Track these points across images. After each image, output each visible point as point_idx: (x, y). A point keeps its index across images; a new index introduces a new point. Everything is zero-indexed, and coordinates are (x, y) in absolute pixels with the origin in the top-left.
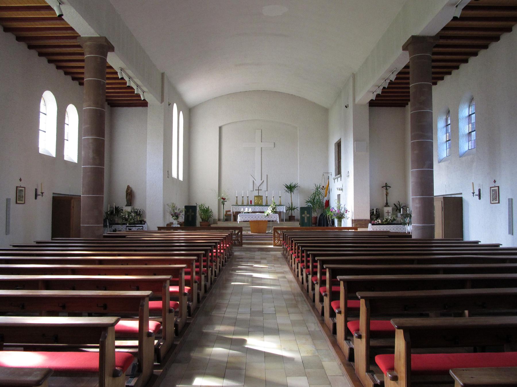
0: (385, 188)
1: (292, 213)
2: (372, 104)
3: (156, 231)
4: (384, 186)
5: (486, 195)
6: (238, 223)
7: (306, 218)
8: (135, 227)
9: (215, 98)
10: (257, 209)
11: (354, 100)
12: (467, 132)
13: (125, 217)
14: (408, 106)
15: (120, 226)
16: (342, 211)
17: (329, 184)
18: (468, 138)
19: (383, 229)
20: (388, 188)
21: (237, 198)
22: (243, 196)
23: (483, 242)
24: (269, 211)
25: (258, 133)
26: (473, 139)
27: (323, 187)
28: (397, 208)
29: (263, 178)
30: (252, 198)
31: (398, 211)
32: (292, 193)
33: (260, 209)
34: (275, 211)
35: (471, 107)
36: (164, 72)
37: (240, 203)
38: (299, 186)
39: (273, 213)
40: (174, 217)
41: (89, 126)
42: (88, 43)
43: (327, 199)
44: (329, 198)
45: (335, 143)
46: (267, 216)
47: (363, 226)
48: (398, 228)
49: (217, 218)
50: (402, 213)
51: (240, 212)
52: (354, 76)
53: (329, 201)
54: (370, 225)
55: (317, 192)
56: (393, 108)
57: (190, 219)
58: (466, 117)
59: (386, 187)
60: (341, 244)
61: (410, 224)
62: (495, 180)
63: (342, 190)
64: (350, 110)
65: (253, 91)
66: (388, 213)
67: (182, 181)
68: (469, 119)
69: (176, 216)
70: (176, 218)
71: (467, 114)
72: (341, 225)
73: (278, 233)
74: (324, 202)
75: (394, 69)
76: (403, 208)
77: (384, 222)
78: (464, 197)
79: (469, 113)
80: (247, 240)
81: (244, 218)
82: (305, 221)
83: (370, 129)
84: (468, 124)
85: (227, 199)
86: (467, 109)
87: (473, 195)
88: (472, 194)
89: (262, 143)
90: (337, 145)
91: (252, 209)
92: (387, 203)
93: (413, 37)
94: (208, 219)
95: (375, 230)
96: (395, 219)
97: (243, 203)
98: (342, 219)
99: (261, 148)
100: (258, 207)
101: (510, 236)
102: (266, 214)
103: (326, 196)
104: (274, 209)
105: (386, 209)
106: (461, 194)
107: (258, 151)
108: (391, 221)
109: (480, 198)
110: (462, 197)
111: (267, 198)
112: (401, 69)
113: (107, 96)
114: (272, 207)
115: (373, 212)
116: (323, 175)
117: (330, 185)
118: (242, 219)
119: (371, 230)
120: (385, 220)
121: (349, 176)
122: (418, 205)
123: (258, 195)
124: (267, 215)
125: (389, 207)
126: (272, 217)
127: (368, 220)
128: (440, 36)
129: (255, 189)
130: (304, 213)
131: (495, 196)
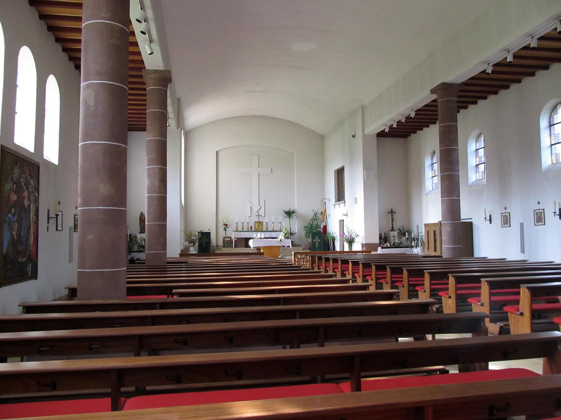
0: (391, 213)
2: (381, 135)
3: (178, 258)
5: (497, 219)
6: (252, 248)
9: (211, 122)
11: (363, 131)
12: (475, 165)
13: (142, 244)
15: (136, 253)
16: (353, 235)
17: (326, 210)
18: (475, 170)
19: (398, 252)
20: (393, 213)
21: (237, 224)
22: (237, 222)
23: (509, 259)
24: (281, 236)
25: (256, 158)
26: (480, 171)
27: (322, 212)
28: (402, 233)
29: (260, 204)
31: (403, 235)
32: (291, 218)
34: (287, 237)
35: (477, 143)
36: (180, 98)
39: (285, 238)
42: (153, 76)
43: (324, 224)
44: (326, 222)
45: (335, 170)
47: (373, 249)
48: (405, 251)
50: (407, 237)
51: (253, 238)
52: (363, 108)
54: (379, 248)
55: (315, 218)
57: (204, 245)
58: (474, 151)
59: (392, 212)
60: (257, 271)
61: (418, 247)
62: (505, 207)
63: (347, 215)
64: (359, 140)
66: (394, 237)
68: (476, 153)
69: (192, 242)
70: (193, 245)
71: (475, 149)
72: (352, 250)
73: (298, 258)
74: (322, 227)
75: (415, 107)
76: (408, 233)
77: (392, 246)
78: (473, 222)
79: (476, 148)
81: (258, 243)
82: (316, 245)
83: (378, 159)
84: (475, 157)
85: (229, 225)
86: (475, 144)
87: (486, 220)
88: (485, 219)
90: (337, 172)
91: (264, 235)
92: (392, 228)
93: (443, 84)
96: (402, 242)
97: (243, 229)
98: (352, 243)
99: (259, 173)
101: (522, 254)
102: (279, 240)
103: (323, 221)
105: (392, 233)
106: (471, 219)
108: (398, 244)
109: (491, 222)
110: (472, 222)
111: (244, 223)
112: (420, 107)
113: (129, 124)
114: (284, 232)
115: (382, 236)
116: (322, 201)
118: (269, 244)
119: (381, 253)
121: (356, 202)
122: (449, 229)
124: (280, 240)
126: (284, 243)
127: (378, 244)
128: (465, 84)
131: (506, 221)
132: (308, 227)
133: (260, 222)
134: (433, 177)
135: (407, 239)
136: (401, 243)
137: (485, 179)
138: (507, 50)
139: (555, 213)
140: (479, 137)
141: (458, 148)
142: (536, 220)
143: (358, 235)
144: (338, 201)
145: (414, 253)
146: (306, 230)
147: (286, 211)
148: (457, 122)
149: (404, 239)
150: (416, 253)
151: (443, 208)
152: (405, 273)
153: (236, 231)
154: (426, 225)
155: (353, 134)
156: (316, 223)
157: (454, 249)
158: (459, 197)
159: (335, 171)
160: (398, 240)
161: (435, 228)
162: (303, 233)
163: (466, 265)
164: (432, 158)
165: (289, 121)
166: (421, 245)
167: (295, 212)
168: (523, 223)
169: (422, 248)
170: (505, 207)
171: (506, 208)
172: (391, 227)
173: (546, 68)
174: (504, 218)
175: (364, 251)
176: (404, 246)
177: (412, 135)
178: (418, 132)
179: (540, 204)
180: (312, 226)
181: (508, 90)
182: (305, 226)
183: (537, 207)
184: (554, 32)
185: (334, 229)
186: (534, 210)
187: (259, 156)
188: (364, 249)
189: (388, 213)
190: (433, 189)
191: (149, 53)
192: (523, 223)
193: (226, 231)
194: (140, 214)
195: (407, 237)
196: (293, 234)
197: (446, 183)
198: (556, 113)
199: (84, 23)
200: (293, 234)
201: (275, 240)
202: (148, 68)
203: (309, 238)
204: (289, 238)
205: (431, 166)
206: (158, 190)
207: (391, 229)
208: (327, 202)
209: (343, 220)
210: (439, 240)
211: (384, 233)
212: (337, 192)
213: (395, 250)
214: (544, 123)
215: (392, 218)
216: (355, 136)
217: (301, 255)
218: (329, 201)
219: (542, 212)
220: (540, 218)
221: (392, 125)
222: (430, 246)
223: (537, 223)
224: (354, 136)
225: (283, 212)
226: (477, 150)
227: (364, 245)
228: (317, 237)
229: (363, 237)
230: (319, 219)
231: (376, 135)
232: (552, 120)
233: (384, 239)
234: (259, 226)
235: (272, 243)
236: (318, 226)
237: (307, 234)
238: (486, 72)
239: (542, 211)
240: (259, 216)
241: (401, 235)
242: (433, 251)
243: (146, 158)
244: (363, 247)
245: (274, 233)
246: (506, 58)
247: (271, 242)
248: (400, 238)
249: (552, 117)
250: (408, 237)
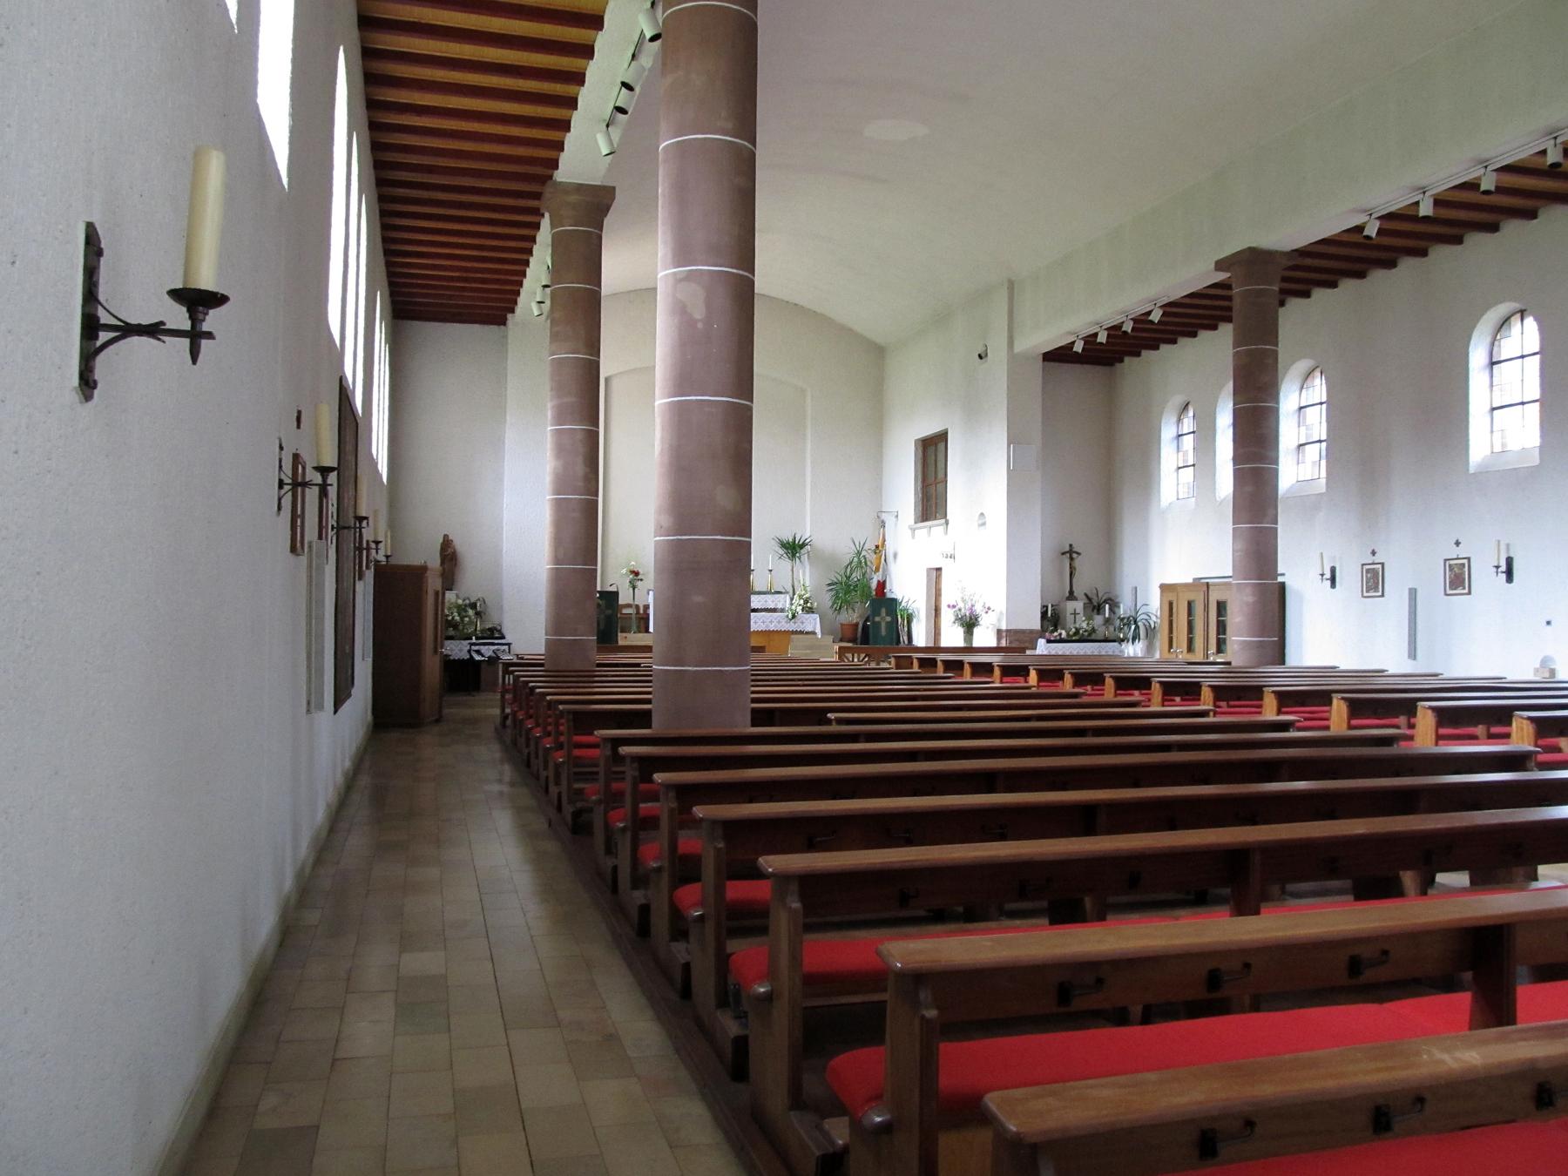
0: (1068, 555)
2: (1059, 356)
4: (1067, 552)
5: (1351, 578)
7: (883, 625)
8: (487, 647)
14: (1122, 364)
16: (978, 609)
17: (884, 541)
18: (1296, 457)
20: (1075, 555)
28: (1094, 607)
34: (810, 608)
35: (1304, 391)
41: (574, 399)
42: (573, 198)
43: (880, 578)
50: (1107, 615)
53: (884, 582)
54: (1041, 642)
55: (859, 562)
56: (1087, 367)
59: (1071, 553)
62: (1373, 550)
64: (998, 368)
72: (972, 644)
74: (874, 585)
86: (1297, 393)
92: (1071, 592)
93: (1252, 250)
95: (1053, 653)
101: (1411, 662)
103: (877, 569)
110: (1284, 583)
120: (1074, 630)
121: (984, 524)
122: (1250, 599)
125: (1077, 600)
126: (803, 623)
127: (1037, 631)
128: (1302, 253)
130: (879, 615)
131: (1374, 581)
134: (1180, 468)
135: (1107, 621)
136: (1094, 630)
137: (1323, 481)
138: (1419, 189)
139: (1497, 567)
140: (1308, 375)
141: (1276, 406)
142: (1450, 582)
143: (989, 608)
144: (923, 521)
145: (1126, 655)
148: (1277, 345)
149: (1098, 620)
150: (1132, 654)
151: (1239, 547)
152: (1207, 694)
154: (1165, 588)
155: (980, 350)
157: (1261, 645)
158: (1276, 523)
159: (916, 441)
160: (1086, 622)
161: (1191, 596)
163: (1276, 678)
164: (1179, 420)
165: (796, 304)
166: (1145, 634)
168: (1415, 589)
169: (1146, 642)
170: (1373, 550)
171: (1374, 553)
172: (1068, 589)
173: (1493, 228)
174: (1369, 575)
175: (1002, 648)
176: (1099, 638)
177: (1127, 359)
178: (1144, 353)
179: (1460, 546)
181: (1394, 270)
183: (1453, 552)
184: (1540, 160)
185: (907, 588)
186: (1446, 560)
188: (1004, 643)
189: (1063, 554)
190: (1178, 499)
191: (605, 152)
192: (1415, 589)
193: (634, 589)
194: (441, 540)
195: (1107, 615)
197: (1249, 489)
198: (1507, 334)
199: (664, 141)
202: (562, 178)
204: (813, 612)
205: (1176, 442)
206: (580, 484)
207: (1067, 594)
209: (939, 570)
210: (1202, 624)
211: (1052, 606)
213: (1071, 647)
214: (1477, 356)
215: (1070, 568)
216: (986, 355)
217: (856, 655)
218: (894, 519)
219: (1463, 565)
220: (1458, 578)
221: (1096, 335)
222: (1174, 640)
223: (1451, 588)
224: (983, 355)
226: (1303, 410)
227: (1004, 634)
228: (883, 611)
229: (1001, 613)
230: (869, 563)
231: (1041, 357)
232: (1495, 349)
233: (1051, 620)
235: (771, 622)
238: (1365, 233)
239: (1465, 561)
241: (1093, 610)
242: (1185, 651)
243: (549, 405)
244: (999, 639)
245: (769, 596)
246: (1417, 203)
248: (1089, 618)
249: (1496, 343)
250: (1109, 615)
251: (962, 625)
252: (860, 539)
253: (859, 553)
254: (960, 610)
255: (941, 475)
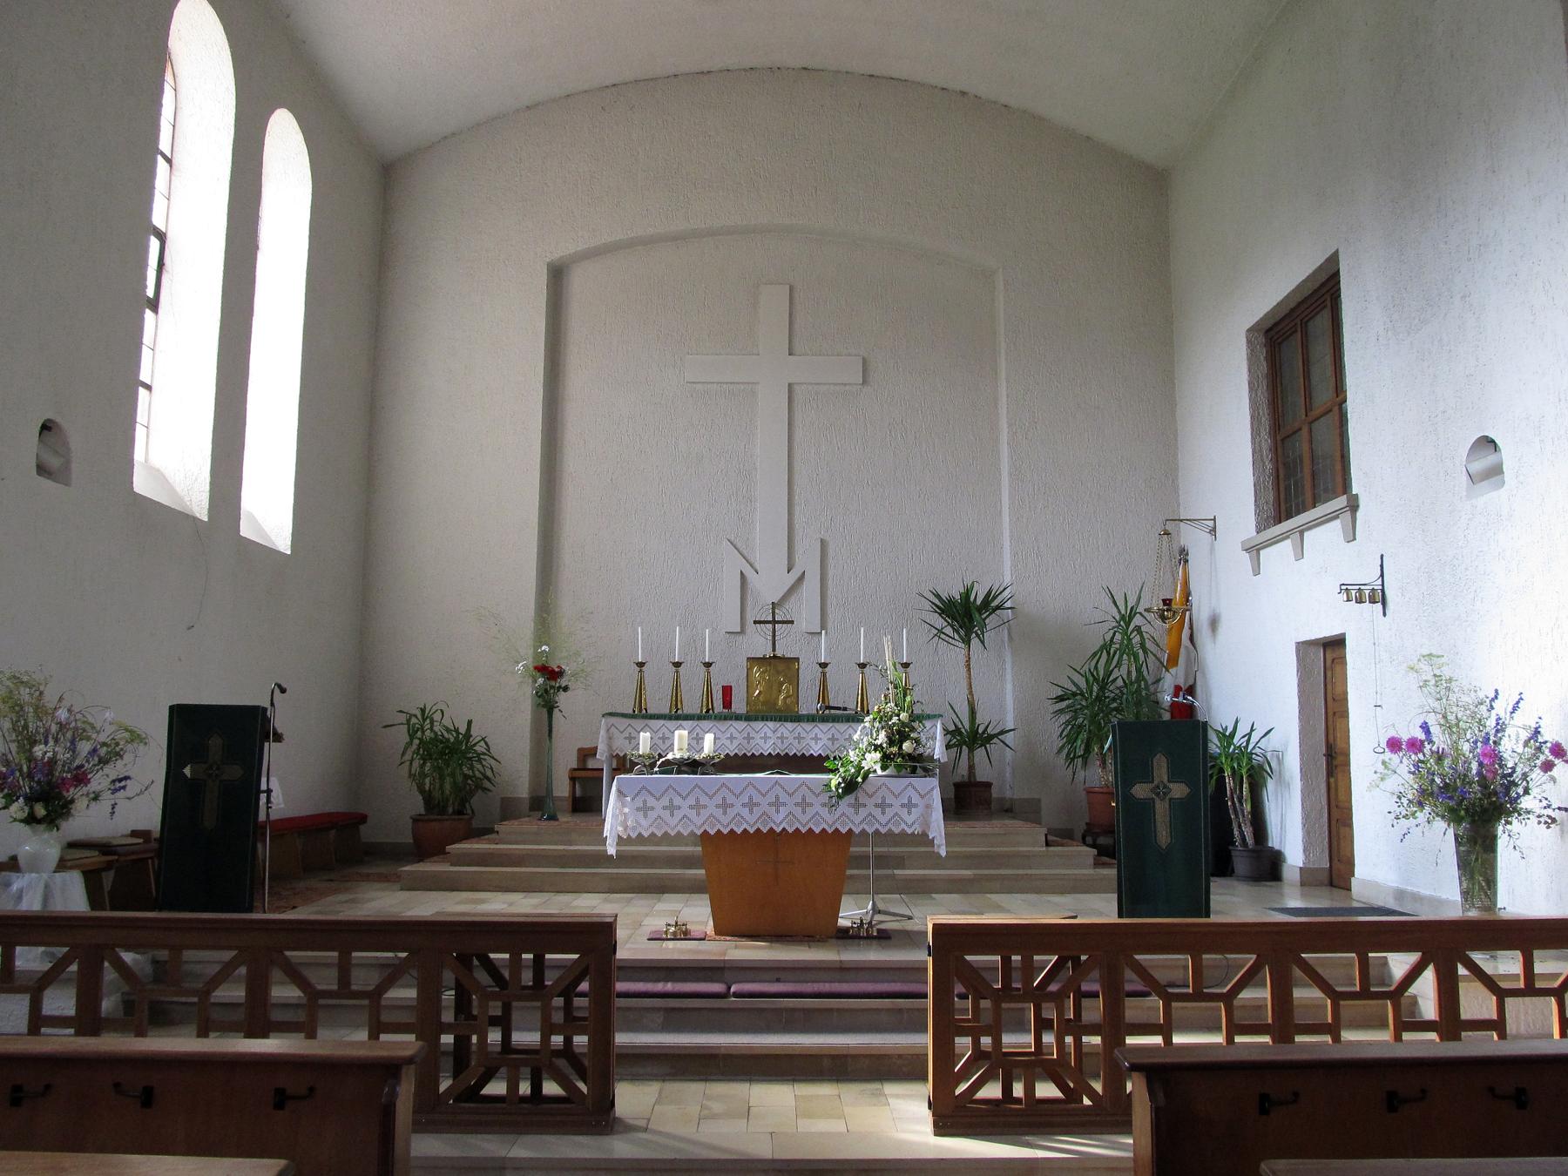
1: (971, 767)
10: (765, 738)
30: (732, 673)
33: (782, 738)
37: (658, 701)
38: (1008, 605)
40: (14, 807)
44: (1195, 665)
46: (849, 799)
49: (523, 791)
63: (1379, 598)
65: (745, 70)
67: (271, 553)
80: (675, 1020)
81: (685, 806)
89: (790, 357)
90: (1262, 339)
94: (464, 801)
97: (676, 700)
99: (790, 385)
100: (771, 724)
103: (1173, 661)
104: (904, 737)
107: (771, 404)
114: (883, 718)
117: (1194, 598)
121: (1496, 471)
123: (769, 653)
126: (882, 806)
129: (750, 619)
130: (1147, 776)
132: (1082, 694)
133: (783, 659)
144: (1279, 520)
146: (1064, 718)
147: (944, 596)
153: (633, 716)
156: (1129, 672)
162: (1051, 731)
167: (998, 607)
180: (1103, 688)
182: (1060, 693)
187: (791, 289)
196: (991, 737)
200: (991, 737)
201: (750, 783)
203: (1085, 764)
208: (1193, 538)
212: (1269, 466)
225: (928, 606)
228: (1161, 767)
230: (1149, 645)
234: (773, 687)
235: (777, 804)
236: (1139, 689)
237: (1071, 740)
240: (774, 622)
247: (718, 800)
251: (1453, 816)
252: (1128, 590)
253: (1127, 618)
254: (1440, 757)
255: (1323, 396)
